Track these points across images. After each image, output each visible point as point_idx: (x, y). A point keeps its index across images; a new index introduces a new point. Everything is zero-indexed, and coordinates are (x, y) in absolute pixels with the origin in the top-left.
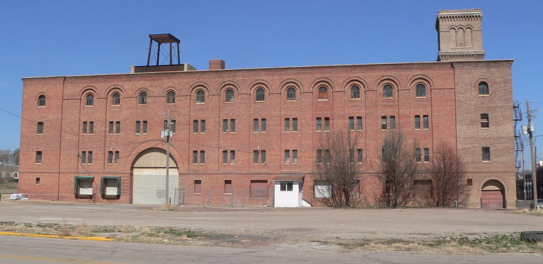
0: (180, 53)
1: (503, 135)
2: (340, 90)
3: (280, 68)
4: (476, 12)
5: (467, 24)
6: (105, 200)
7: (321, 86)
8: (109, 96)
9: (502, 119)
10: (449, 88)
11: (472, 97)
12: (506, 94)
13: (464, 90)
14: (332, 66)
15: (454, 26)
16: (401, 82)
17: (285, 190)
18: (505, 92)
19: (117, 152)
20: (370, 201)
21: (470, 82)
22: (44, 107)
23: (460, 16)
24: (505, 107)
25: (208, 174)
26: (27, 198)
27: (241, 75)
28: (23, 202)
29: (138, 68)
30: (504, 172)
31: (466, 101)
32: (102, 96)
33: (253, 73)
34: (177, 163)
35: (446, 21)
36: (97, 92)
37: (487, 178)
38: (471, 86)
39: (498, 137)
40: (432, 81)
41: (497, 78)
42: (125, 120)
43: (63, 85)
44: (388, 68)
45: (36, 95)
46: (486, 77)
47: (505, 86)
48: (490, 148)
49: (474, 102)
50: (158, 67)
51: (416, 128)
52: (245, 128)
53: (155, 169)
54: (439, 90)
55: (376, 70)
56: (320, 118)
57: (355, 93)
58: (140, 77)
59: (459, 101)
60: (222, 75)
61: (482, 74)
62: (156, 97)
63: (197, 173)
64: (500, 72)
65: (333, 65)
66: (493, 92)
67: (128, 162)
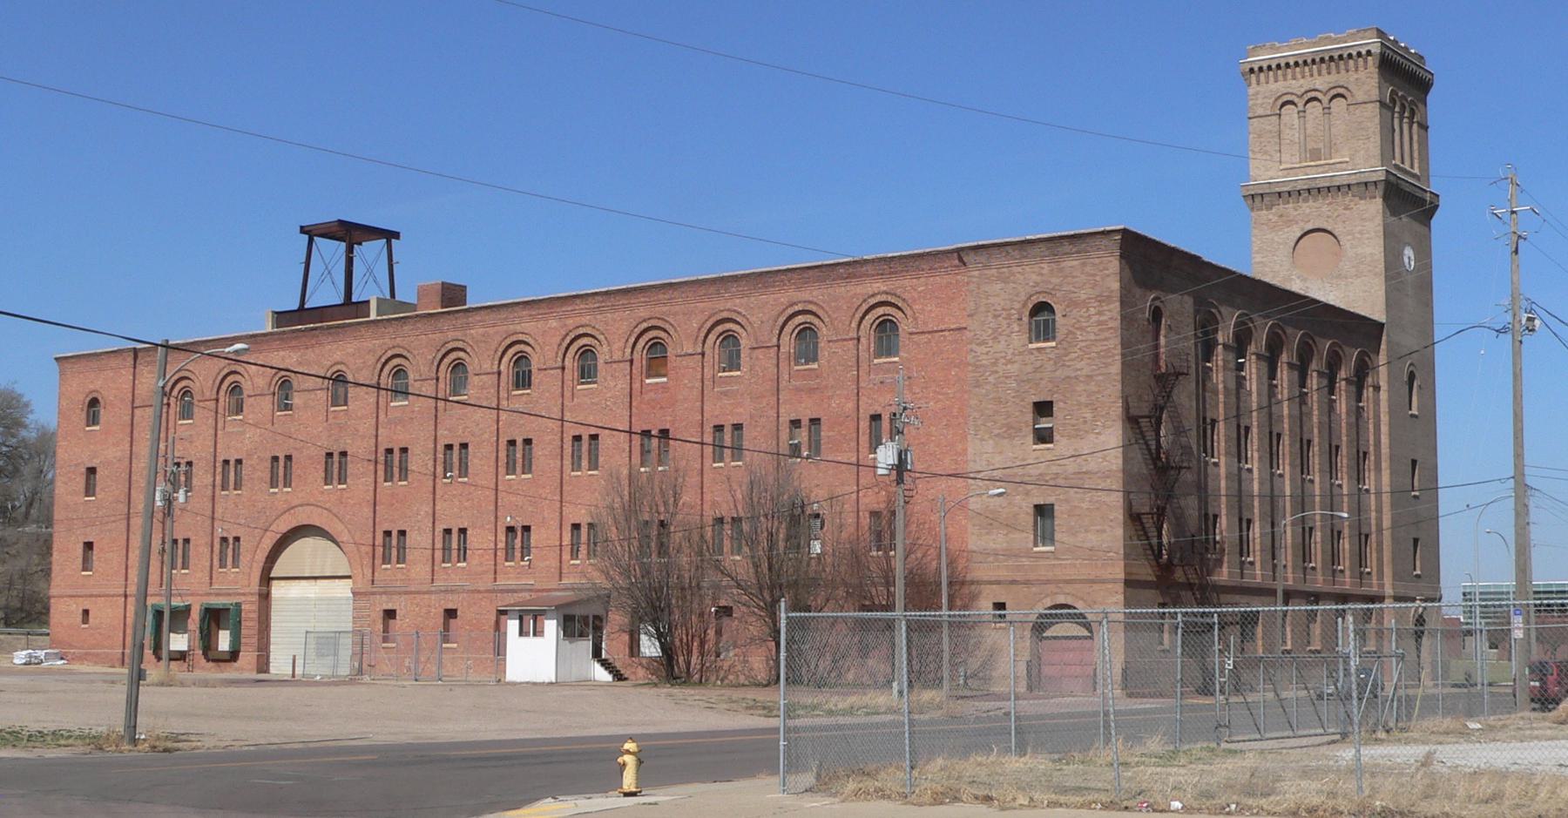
0: (395, 266)
2: (690, 351)
3: (558, 298)
4: (1362, 39)
5: (1332, 85)
6: (211, 664)
7: (652, 342)
8: (222, 393)
9: (1089, 416)
10: (953, 327)
11: (1011, 351)
12: (1102, 337)
13: (990, 331)
14: (671, 285)
15: (1292, 94)
16: (836, 319)
17: (527, 634)
18: (1100, 330)
19: (237, 539)
20: (756, 666)
21: (1008, 307)
22: (96, 428)
23: (1309, 61)
24: (1100, 378)
25: (411, 593)
26: (62, 662)
27: (480, 321)
28: (49, 671)
29: (281, 317)
30: (1093, 582)
31: (995, 364)
32: (551, 364)
33: (504, 314)
35: (1267, 83)
36: (749, 329)
37: (1044, 601)
38: (1009, 317)
39: (1079, 473)
40: (911, 307)
42: (250, 455)
43: (132, 370)
44: (803, 278)
45: (82, 399)
46: (1051, 287)
47: (1100, 313)
48: (1056, 507)
49: (1016, 366)
50: (322, 313)
52: (486, 468)
53: (313, 582)
55: (774, 286)
56: (799, 421)
57: (730, 358)
58: (279, 339)
59: (977, 367)
60: (440, 325)
61: (1039, 279)
62: (308, 391)
63: (389, 589)
64: (1088, 269)
65: (673, 281)
66: (1067, 334)
67: (255, 565)
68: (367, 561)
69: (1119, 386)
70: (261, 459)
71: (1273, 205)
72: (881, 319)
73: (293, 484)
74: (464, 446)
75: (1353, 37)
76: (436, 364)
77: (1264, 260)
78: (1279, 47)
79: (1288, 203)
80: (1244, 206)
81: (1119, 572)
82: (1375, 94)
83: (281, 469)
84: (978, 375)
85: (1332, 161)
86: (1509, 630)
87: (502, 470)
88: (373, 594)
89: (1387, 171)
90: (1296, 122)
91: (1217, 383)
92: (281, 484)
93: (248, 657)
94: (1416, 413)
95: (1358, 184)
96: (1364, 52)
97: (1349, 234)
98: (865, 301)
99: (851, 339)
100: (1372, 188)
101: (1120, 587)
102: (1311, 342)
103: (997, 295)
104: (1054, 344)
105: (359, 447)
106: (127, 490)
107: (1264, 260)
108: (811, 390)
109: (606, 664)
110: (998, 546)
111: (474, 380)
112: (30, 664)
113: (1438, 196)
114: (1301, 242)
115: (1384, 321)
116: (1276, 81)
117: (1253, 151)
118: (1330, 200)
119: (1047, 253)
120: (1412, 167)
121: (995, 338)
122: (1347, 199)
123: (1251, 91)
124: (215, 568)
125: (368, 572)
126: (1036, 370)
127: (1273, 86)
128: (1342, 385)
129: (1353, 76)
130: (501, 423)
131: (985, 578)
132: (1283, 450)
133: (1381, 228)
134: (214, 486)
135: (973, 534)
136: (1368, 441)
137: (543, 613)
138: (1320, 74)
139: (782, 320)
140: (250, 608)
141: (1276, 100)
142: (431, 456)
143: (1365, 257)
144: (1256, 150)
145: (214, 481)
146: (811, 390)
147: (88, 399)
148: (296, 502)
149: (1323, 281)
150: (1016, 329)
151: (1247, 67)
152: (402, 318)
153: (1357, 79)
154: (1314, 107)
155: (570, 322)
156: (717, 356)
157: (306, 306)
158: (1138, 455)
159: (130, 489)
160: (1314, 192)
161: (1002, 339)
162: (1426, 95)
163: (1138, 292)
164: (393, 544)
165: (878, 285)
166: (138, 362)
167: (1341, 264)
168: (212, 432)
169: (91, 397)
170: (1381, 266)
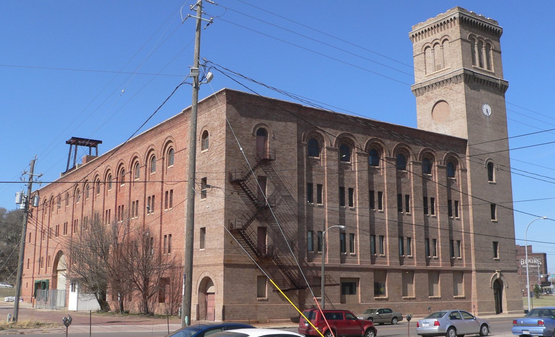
1: (216, 208)
5: (443, 35)
12: (220, 143)
15: (428, 43)
34: (115, 191)
47: (220, 132)
48: (206, 229)
55: (145, 140)
71: (423, 93)
72: (169, 150)
82: (459, 36)
85: (444, 69)
89: (464, 69)
91: (324, 167)
94: (495, 182)
100: (459, 78)
101: (222, 267)
102: (407, 148)
113: (508, 82)
114: (435, 108)
120: (489, 68)
122: (451, 85)
129: (450, 29)
133: (464, 96)
138: (438, 32)
141: (423, 47)
143: (459, 110)
149: (443, 124)
153: (452, 31)
154: (437, 47)
162: (499, 38)
163: (243, 120)
167: (450, 115)
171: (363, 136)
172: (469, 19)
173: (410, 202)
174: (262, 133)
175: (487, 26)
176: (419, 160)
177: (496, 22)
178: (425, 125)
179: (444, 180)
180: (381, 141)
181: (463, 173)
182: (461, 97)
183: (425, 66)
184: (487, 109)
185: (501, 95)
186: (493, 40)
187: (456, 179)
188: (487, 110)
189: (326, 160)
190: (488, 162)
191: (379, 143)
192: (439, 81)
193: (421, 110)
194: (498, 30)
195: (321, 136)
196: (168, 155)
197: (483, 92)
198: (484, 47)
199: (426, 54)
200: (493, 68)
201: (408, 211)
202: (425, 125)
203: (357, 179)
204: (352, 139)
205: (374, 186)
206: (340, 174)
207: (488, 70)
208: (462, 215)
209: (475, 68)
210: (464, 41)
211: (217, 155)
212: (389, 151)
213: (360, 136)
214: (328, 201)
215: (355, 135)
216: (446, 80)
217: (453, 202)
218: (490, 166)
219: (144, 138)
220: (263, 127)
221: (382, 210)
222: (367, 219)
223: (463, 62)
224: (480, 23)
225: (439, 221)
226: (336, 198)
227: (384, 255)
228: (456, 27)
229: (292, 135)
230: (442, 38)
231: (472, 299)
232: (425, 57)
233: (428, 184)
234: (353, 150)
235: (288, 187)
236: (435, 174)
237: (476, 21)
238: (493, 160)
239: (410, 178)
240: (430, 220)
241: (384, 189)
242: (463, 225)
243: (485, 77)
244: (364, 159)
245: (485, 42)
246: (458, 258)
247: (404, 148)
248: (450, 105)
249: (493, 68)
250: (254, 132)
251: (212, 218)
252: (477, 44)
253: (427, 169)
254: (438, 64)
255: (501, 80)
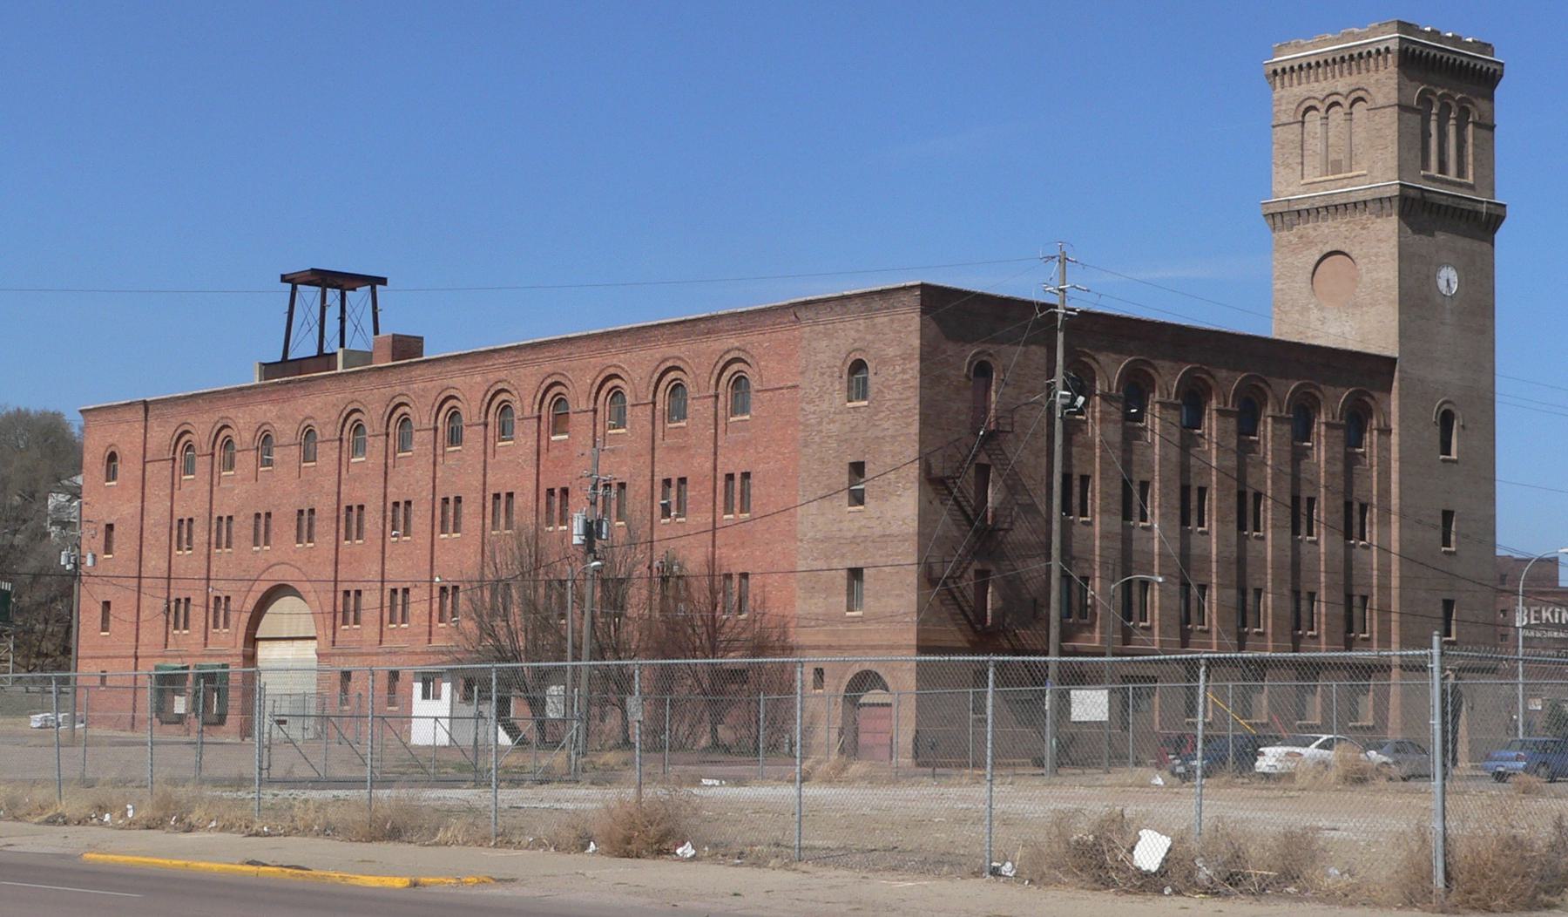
1: (894, 529)
4: (1383, 34)
5: (1353, 87)
7: (674, 383)
12: (904, 396)
13: (817, 389)
15: (1314, 98)
17: (429, 698)
21: (831, 364)
22: (114, 483)
24: (902, 438)
27: (421, 376)
29: (268, 369)
31: (820, 423)
35: (1291, 86)
39: (884, 536)
41: (890, 346)
47: (904, 372)
49: (837, 425)
50: (302, 365)
51: (725, 514)
53: (290, 642)
54: (770, 393)
55: (650, 342)
58: (262, 392)
59: (807, 426)
65: (570, 336)
68: (329, 622)
69: (917, 447)
70: (247, 517)
72: (734, 378)
73: (272, 543)
74: (408, 503)
75: (1374, 32)
76: (386, 419)
77: (1284, 286)
78: (1303, 46)
79: (1308, 222)
80: (1265, 225)
81: (911, 638)
83: (263, 525)
84: (807, 434)
85: (1350, 175)
86: (918, 689)
87: (437, 529)
88: (333, 655)
90: (1319, 129)
92: (305, 540)
93: (233, 720)
95: (1373, 200)
96: (1382, 50)
97: (1364, 258)
98: (721, 357)
99: (710, 396)
100: (1387, 205)
102: (1262, 385)
103: (823, 353)
104: (866, 403)
105: (325, 506)
106: (138, 548)
107: (1284, 286)
108: (681, 449)
109: (512, 730)
110: (820, 611)
111: (417, 436)
112: (47, 727)
113: (1504, 206)
115: (1397, 355)
116: (1299, 84)
117: (1276, 164)
118: (1348, 218)
119: (863, 309)
120: (1461, 172)
121: (821, 396)
122: (1365, 217)
123: (1275, 96)
124: (385, 624)
125: (330, 632)
126: (853, 430)
127: (1296, 89)
128: (1319, 428)
129: (1373, 77)
130: (437, 480)
131: (808, 643)
132: (1210, 505)
133: (1396, 250)
134: (209, 544)
135: (799, 597)
136: (1371, 492)
137: (439, 675)
139: (656, 376)
140: (236, 670)
141: (1299, 105)
142: (380, 514)
144: (1279, 163)
145: (210, 538)
146: (681, 449)
147: (108, 453)
148: (273, 561)
149: (1339, 311)
150: (838, 387)
151: (1271, 68)
152: (358, 371)
153: (1377, 80)
154: (1337, 112)
155: (491, 376)
156: (607, 413)
157: (289, 358)
158: (944, 517)
159: (141, 546)
160: (1332, 210)
161: (827, 397)
163: (951, 348)
164: (347, 606)
165: (732, 341)
166: (150, 414)
167: (1358, 290)
168: (208, 487)
169: (110, 451)
170: (1395, 294)
171: (1172, 364)
172: (1421, 52)
173: (1262, 508)
174: (983, 370)
175: (1465, 63)
176: (1287, 413)
177: (1490, 45)
178: (1292, 306)
179: (1338, 456)
180: (1208, 373)
181: (1382, 437)
182: (1390, 248)
183: (1302, 156)
184: (1448, 279)
185: (1483, 240)
186: (1476, 98)
187: (1365, 452)
188: (1448, 281)
189: (1098, 421)
190: (1442, 409)
191: (1204, 376)
192: (1336, 203)
193: (1283, 267)
194: (1491, 70)
195: (1091, 368)
196: (729, 390)
197: (1441, 237)
198: (1454, 118)
199: (1306, 125)
200: (1471, 172)
201: (1257, 529)
202: (1292, 306)
203: (1157, 461)
204: (1152, 371)
205: (1192, 475)
206: (1124, 451)
207: (1458, 180)
208: (1375, 538)
209: (1427, 178)
210: (1406, 111)
211: (894, 418)
212: (1224, 395)
213: (1167, 364)
214: (1102, 511)
215: (1156, 362)
216: (1355, 203)
217: (1356, 506)
218: (1446, 419)
219: (647, 335)
220: (985, 358)
221: (1206, 529)
222: (1174, 549)
223: (1399, 166)
224: (1448, 59)
225: (1322, 550)
226: (1117, 506)
227: (1206, 627)
228: (1391, 73)
229: (1039, 372)
230: (1350, 93)
231: (1389, 732)
232: (1302, 134)
233: (1304, 464)
234: (1151, 395)
235: (1029, 484)
236: (1319, 443)
237: (1432, 53)
238: (1454, 405)
239: (1265, 454)
240: (1304, 549)
241: (1211, 480)
242: (1375, 561)
243: (1450, 199)
244: (1173, 416)
245: (1457, 106)
246: (1361, 635)
247: (1257, 386)
248: (1359, 267)
249: (1471, 172)
250: (969, 370)
251: (883, 549)
252: (1436, 114)
253: (1303, 429)
254: (1337, 158)
255: (1488, 202)
